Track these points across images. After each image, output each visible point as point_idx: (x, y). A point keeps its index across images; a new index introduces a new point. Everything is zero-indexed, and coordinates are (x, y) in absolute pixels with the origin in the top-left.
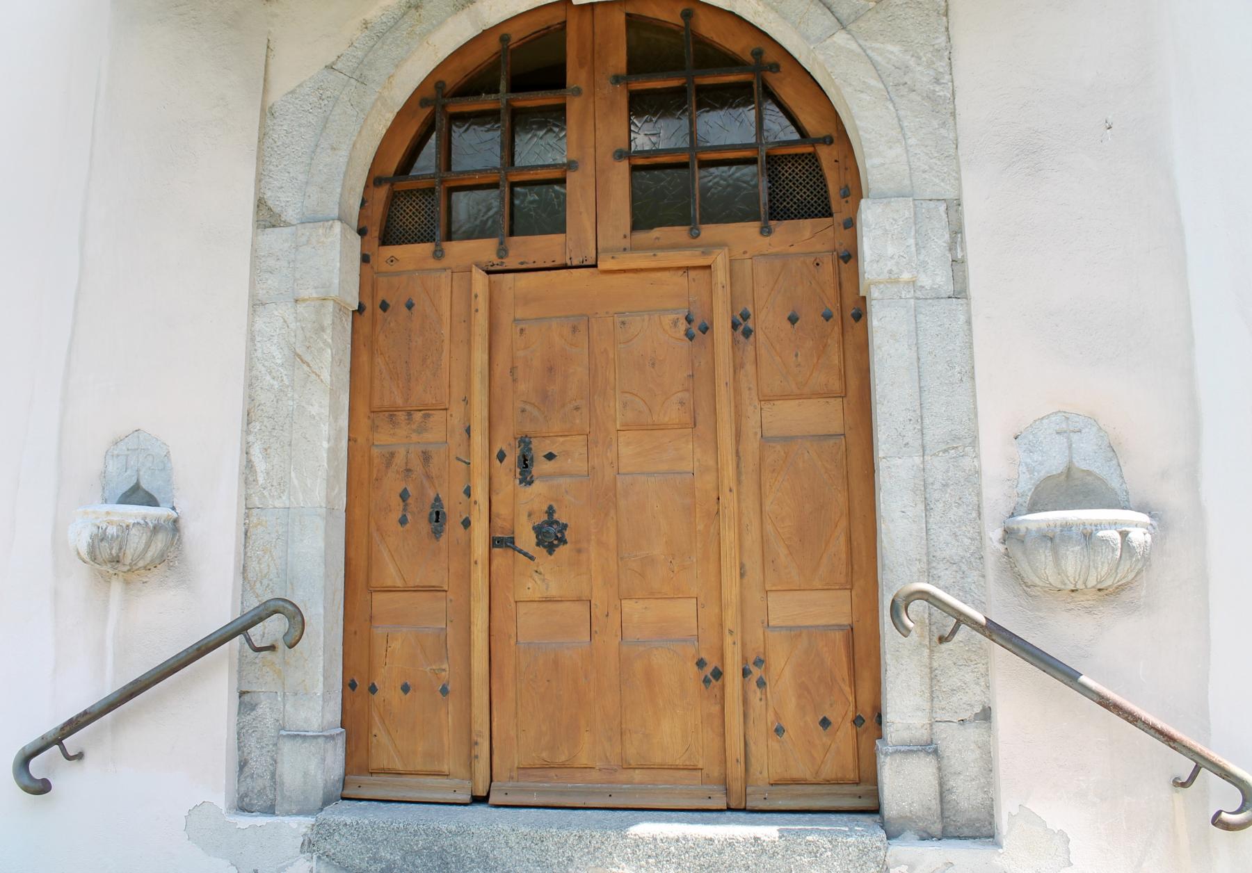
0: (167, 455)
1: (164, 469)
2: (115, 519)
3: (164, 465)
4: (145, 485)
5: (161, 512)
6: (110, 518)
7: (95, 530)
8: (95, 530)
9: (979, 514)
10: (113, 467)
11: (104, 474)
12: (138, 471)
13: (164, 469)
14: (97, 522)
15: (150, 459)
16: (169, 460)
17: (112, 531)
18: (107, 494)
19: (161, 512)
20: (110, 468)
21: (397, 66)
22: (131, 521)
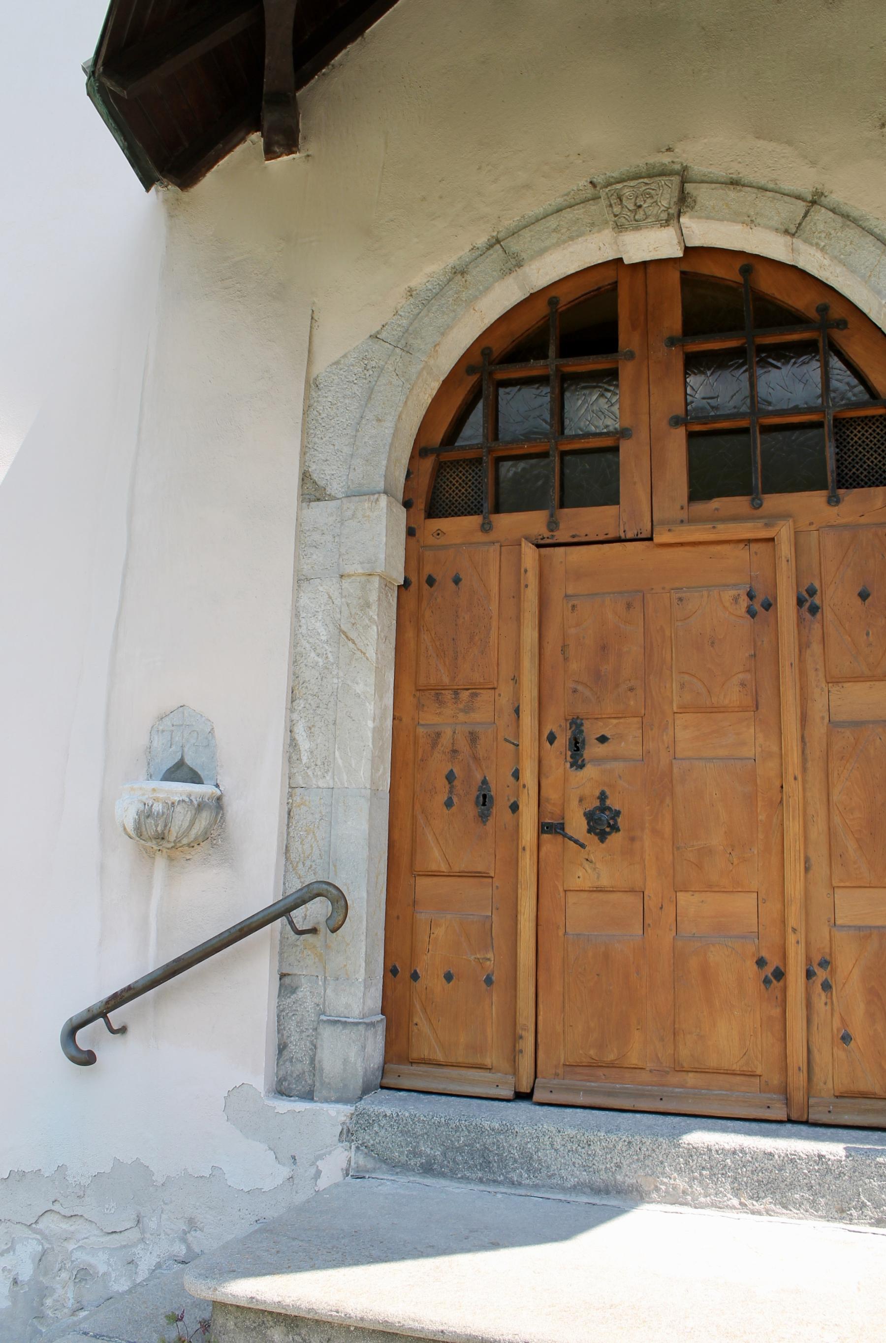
0: (212, 732)
2: (161, 795)
3: (208, 740)
4: (188, 761)
6: (155, 795)
7: (141, 807)
8: (141, 807)
10: (158, 742)
11: (149, 749)
14: (144, 799)
15: (195, 734)
16: (213, 737)
18: (152, 770)
20: (155, 744)
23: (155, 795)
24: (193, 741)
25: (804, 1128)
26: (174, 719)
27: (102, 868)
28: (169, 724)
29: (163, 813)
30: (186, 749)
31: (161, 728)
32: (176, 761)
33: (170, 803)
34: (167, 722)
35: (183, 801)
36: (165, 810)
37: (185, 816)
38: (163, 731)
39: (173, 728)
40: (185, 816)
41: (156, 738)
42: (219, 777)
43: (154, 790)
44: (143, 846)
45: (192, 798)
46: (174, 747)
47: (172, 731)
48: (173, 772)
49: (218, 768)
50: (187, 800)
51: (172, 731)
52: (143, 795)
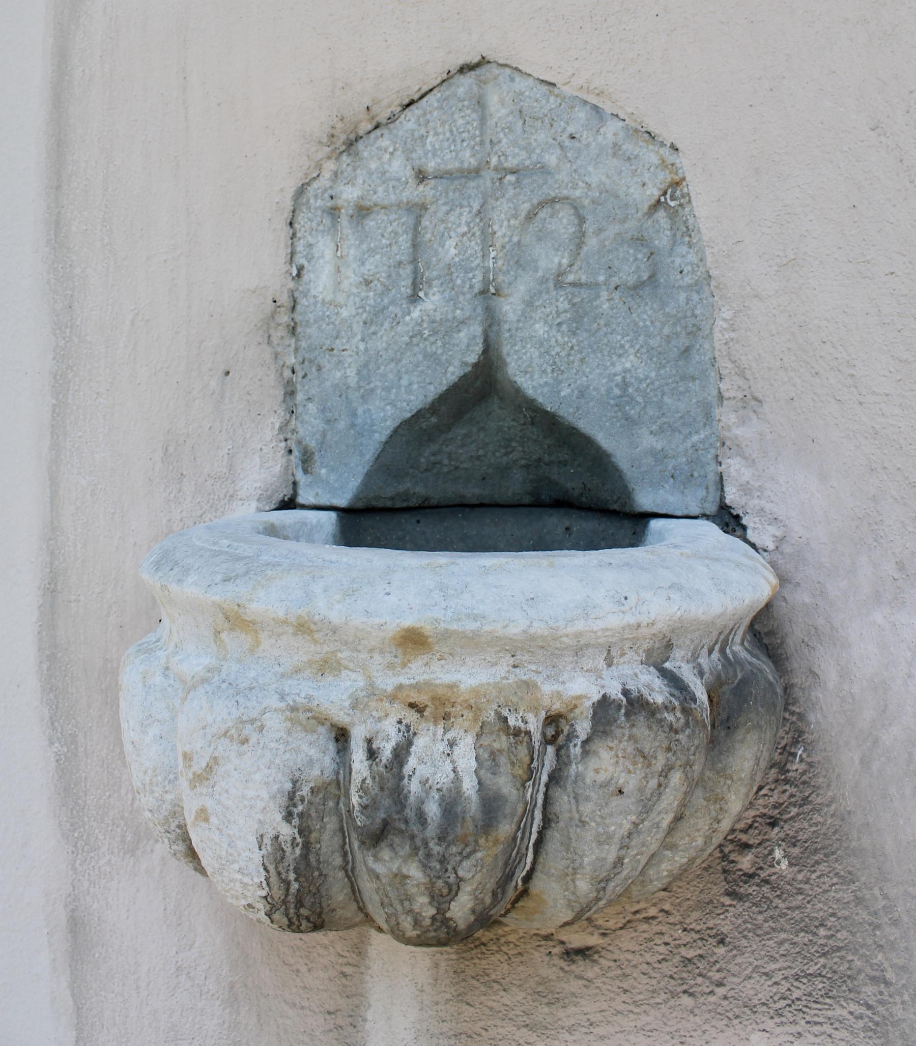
0: (672, 197)
1: (649, 285)
2: (469, 676)
3: (652, 248)
4: (530, 372)
5: (676, 586)
6: (419, 672)
7: (315, 757)
8: (315, 757)
9: (291, 393)
10: (336, 274)
11: (288, 316)
12: (488, 294)
13: (649, 285)
14: (335, 697)
15: (562, 223)
16: (685, 231)
17: (446, 763)
18: (310, 426)
19: (676, 586)
20: (320, 282)
21: (333, 136)
22: (582, 687)
23: (419, 672)
24: (550, 259)
25: (554, 522)
26: (422, 141)
27: (78, 933)
28: (398, 167)
29: (491, 805)
30: (510, 308)
31: (349, 194)
32: (454, 373)
33: (534, 725)
34: (386, 164)
35: (636, 704)
36: (505, 784)
37: (646, 807)
38: (362, 211)
39: (426, 191)
40: (646, 807)
41: (324, 247)
42: (733, 467)
43: (413, 641)
44: (295, 838)
45: (679, 664)
46: (433, 301)
47: (418, 210)
48: (429, 436)
49: (727, 416)
50: (658, 693)
51: (418, 210)
52: (326, 667)
